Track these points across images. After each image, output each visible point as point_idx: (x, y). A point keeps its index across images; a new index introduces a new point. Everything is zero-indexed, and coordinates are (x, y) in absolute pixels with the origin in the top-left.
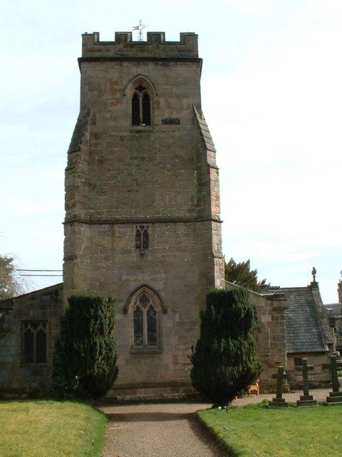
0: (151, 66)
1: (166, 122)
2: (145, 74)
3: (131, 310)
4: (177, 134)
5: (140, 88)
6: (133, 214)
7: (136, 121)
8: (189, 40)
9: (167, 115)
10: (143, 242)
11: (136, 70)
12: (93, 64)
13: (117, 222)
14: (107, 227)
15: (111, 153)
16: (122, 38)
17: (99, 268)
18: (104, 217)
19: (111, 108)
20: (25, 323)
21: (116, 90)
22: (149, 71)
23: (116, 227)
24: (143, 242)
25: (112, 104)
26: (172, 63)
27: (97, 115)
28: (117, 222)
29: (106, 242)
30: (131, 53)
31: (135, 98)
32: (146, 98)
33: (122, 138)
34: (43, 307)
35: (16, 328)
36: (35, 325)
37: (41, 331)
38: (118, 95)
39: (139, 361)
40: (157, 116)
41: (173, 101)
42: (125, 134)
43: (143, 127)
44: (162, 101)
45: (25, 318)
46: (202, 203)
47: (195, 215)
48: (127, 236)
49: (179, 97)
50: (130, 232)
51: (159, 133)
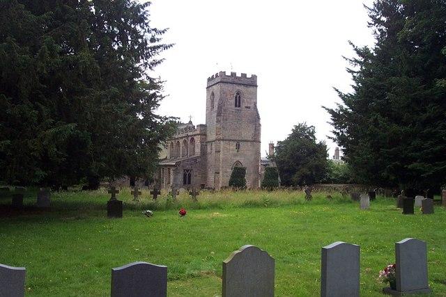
1: (246, 107)
5: (238, 94)
7: (236, 106)
8: (254, 77)
10: (238, 147)
11: (238, 88)
16: (233, 74)
22: (241, 88)
24: (238, 147)
29: (228, 146)
30: (236, 81)
31: (236, 97)
35: (182, 172)
40: (243, 105)
48: (233, 146)
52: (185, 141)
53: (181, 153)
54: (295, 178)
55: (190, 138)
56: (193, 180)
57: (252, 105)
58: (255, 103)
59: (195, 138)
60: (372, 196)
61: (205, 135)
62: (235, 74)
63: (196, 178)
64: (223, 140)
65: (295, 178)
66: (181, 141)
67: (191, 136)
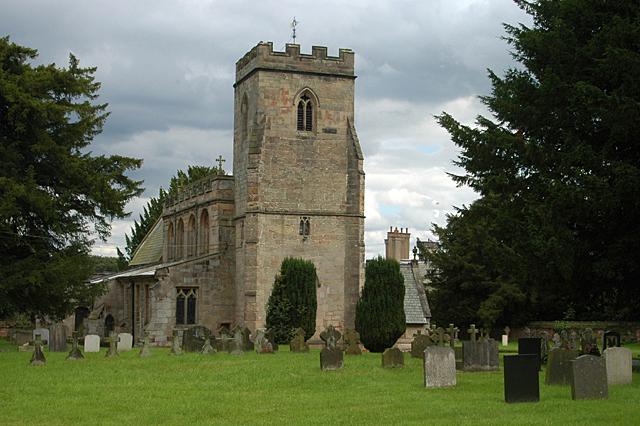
0: (316, 79)
1: (326, 131)
2: (310, 86)
3: (297, 104)
4: (334, 142)
5: (305, 97)
6: (302, 207)
7: (300, 127)
8: (346, 55)
9: (327, 126)
10: (305, 229)
11: (302, 81)
12: (269, 73)
13: (286, 213)
14: (278, 216)
15: (283, 154)
16: (292, 50)
17: (272, 249)
18: (276, 209)
19: (282, 115)
20: (178, 289)
21: (287, 100)
22: (316, 85)
23: (286, 217)
24: (305, 229)
25: (283, 112)
26: (332, 78)
27: (272, 121)
28: (286, 213)
29: (278, 229)
30: (300, 66)
31: (300, 105)
32: (309, 106)
33: (291, 143)
34: (195, 275)
35: (172, 293)
36: (186, 290)
37: (192, 295)
38: (289, 104)
39: (271, 139)
40: (321, 124)
41: (331, 112)
42: (294, 139)
43: (304, 133)
44: (323, 112)
45: (180, 285)
46: (351, 202)
47: (345, 210)
48: (293, 226)
49: (338, 109)
50: (298, 220)
51: (321, 140)
52: (193, 219)
53: (305, 124)
54: (487, 309)
55: (200, 210)
56: (201, 312)
57: (341, 126)
58: (350, 122)
59: (210, 209)
60: (380, 258)
61: (232, 202)
62: (298, 48)
63: (208, 315)
64: (266, 213)
65: (487, 309)
66: (186, 219)
67: (202, 205)
